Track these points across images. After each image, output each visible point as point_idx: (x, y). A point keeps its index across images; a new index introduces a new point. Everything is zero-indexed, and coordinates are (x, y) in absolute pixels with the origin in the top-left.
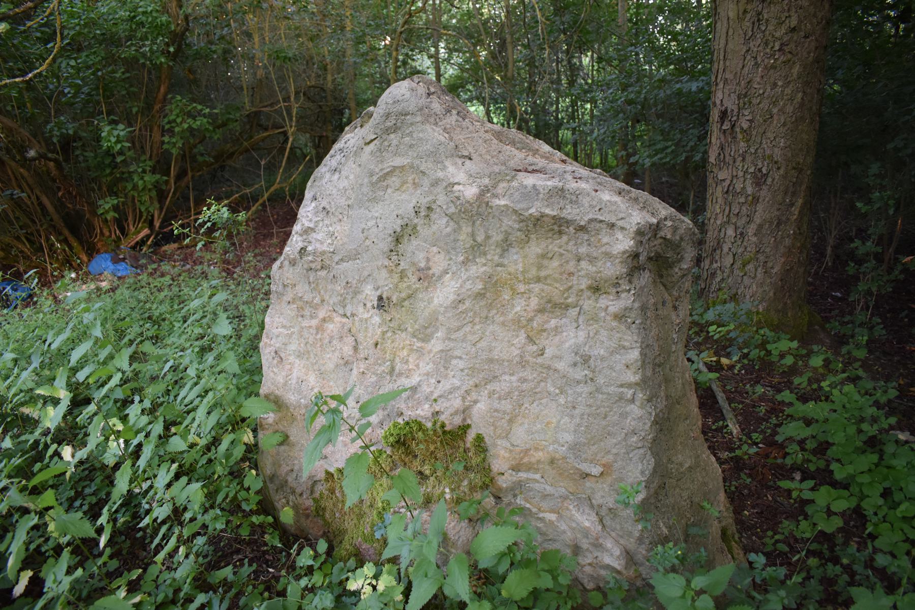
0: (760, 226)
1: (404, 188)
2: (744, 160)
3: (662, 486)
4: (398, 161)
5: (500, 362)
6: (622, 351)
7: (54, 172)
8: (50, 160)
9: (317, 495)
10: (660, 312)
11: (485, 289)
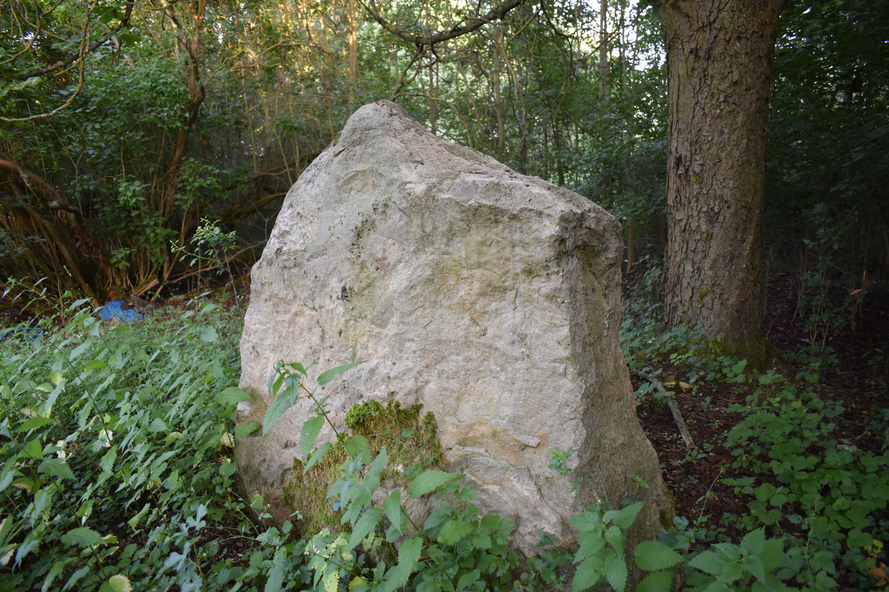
0: (715, 261)
1: (365, 189)
2: (697, 201)
3: (594, 459)
4: (361, 167)
5: (447, 342)
6: (554, 329)
7: (74, 224)
8: (71, 211)
9: (287, 485)
10: (589, 297)
11: (433, 275)
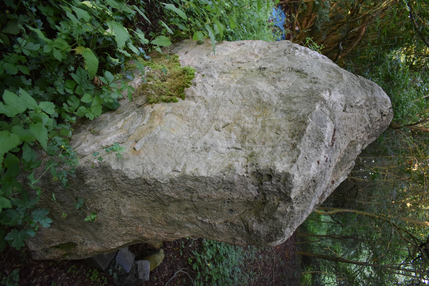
11: (263, 102)
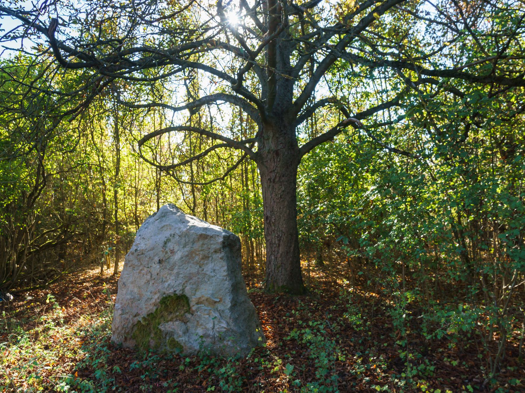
0: (281, 254)
